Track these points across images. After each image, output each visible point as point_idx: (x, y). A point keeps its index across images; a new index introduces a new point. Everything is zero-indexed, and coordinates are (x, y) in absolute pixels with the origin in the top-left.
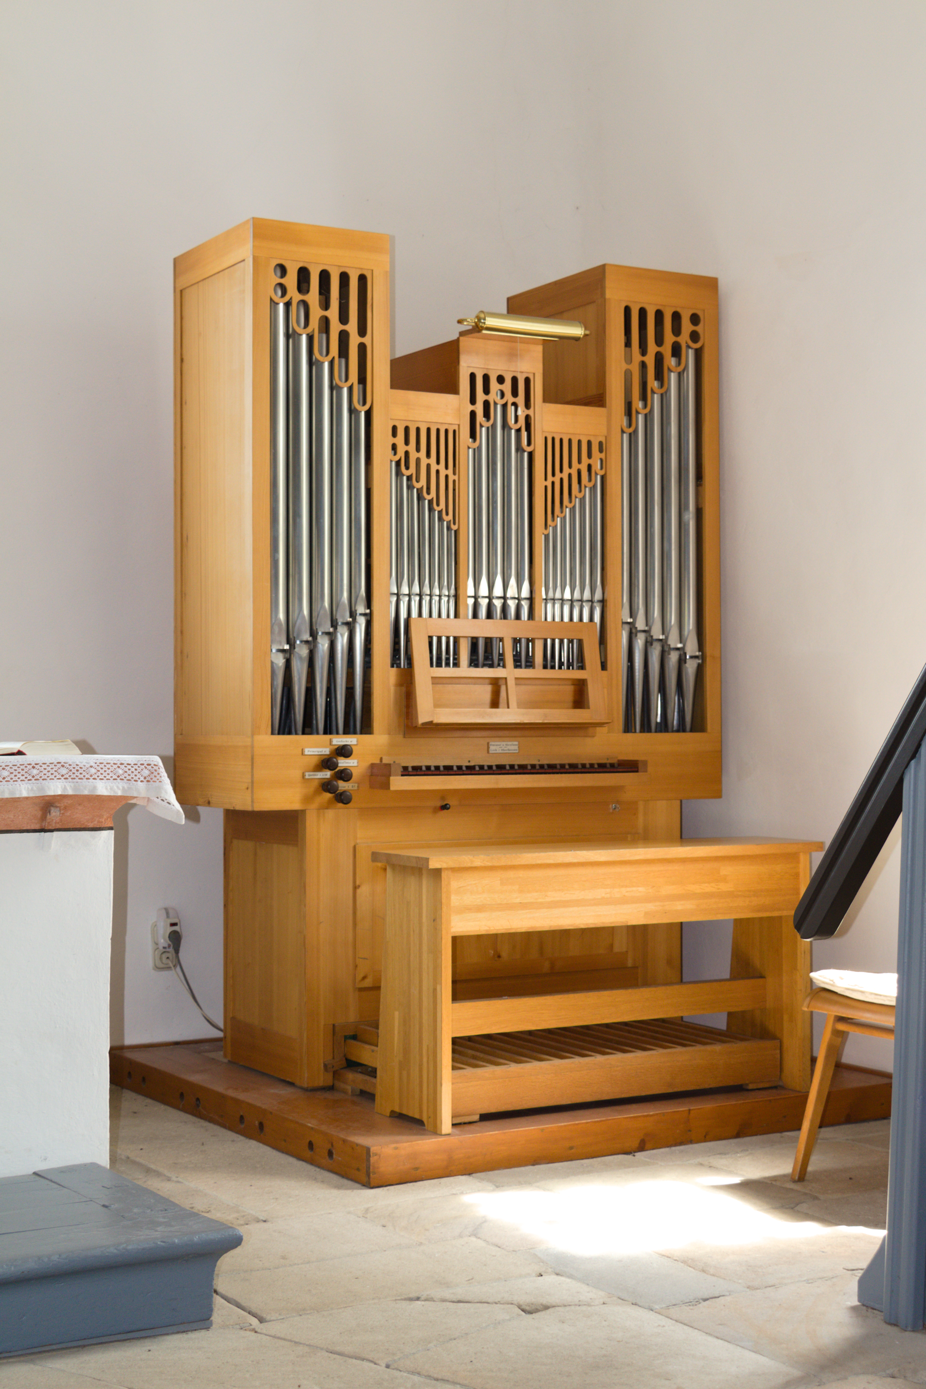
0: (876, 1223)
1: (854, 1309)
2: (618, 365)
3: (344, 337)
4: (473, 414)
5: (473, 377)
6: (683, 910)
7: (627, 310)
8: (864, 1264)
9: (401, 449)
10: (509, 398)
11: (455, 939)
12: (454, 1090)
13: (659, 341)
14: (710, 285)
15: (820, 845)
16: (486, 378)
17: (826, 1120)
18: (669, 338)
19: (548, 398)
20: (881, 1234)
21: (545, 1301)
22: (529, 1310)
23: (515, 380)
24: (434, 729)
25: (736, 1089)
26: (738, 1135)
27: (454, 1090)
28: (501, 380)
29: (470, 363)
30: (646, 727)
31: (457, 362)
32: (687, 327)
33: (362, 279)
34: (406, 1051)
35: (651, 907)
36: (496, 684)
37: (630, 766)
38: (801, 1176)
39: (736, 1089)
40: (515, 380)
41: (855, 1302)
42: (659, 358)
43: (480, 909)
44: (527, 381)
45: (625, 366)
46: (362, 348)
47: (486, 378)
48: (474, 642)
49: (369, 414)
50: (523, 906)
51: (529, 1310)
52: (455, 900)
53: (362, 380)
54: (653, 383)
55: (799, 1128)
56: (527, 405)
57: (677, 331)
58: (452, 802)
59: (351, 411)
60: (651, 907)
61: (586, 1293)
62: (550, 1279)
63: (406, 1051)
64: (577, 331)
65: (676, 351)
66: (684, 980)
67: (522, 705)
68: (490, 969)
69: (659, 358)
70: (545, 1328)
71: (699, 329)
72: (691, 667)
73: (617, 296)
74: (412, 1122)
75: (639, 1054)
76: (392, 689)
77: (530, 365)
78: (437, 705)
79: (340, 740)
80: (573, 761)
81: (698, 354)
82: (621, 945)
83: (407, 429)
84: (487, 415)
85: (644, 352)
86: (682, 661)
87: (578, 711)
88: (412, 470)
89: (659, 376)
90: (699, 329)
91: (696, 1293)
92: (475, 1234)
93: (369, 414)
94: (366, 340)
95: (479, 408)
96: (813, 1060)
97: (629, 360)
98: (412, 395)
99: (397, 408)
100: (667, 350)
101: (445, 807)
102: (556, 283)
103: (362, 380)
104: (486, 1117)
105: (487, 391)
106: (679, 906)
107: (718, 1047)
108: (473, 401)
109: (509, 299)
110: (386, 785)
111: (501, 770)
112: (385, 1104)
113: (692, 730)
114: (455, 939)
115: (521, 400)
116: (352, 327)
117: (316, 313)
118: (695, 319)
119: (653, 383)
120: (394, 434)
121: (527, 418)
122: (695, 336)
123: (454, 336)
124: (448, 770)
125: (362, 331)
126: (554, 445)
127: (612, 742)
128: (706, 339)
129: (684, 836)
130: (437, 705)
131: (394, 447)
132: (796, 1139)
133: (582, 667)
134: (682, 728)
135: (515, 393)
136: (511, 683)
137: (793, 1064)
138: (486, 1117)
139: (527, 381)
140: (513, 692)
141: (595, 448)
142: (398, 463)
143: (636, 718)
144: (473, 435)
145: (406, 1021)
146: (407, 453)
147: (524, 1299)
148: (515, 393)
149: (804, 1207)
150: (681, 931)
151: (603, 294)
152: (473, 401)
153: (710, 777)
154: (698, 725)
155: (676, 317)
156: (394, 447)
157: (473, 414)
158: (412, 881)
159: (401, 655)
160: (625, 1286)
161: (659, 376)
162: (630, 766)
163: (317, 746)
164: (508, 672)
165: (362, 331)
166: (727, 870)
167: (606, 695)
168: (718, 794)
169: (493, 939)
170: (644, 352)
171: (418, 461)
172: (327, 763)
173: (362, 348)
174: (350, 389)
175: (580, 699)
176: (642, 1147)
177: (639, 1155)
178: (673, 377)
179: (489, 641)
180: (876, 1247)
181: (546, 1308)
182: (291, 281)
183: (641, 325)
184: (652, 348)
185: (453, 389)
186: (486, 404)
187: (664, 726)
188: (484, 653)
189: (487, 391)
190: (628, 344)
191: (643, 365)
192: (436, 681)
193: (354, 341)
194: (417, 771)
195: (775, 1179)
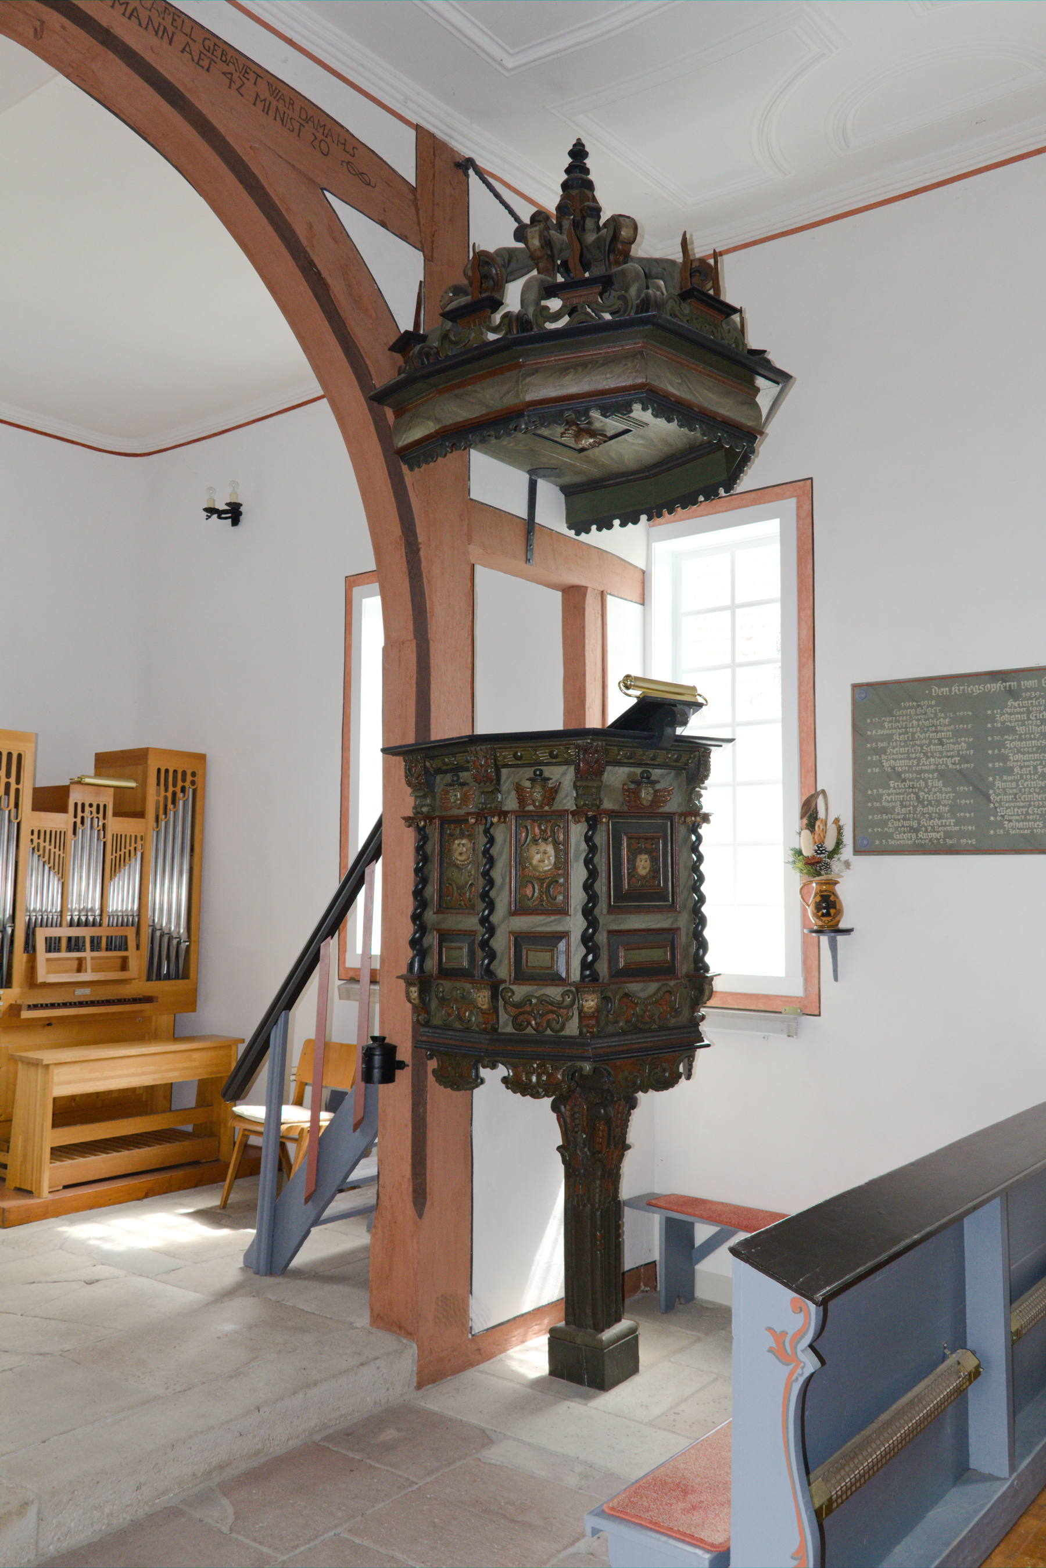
0: (252, 1227)
1: (241, 1268)
2: (153, 797)
4: (75, 823)
5: (76, 804)
6: (171, 1076)
7: (159, 770)
8: (247, 1248)
9: (36, 841)
10: (95, 814)
11: (54, 1099)
12: (51, 1175)
13: (175, 785)
14: (202, 758)
15: (243, 1041)
16: (83, 805)
17: (237, 1176)
18: (180, 784)
19: (116, 814)
20: (254, 1231)
21: (97, 1278)
22: (90, 1283)
23: (98, 806)
24: (45, 985)
25: (195, 1163)
26: (195, 1187)
27: (51, 1175)
28: (91, 805)
29: (76, 796)
30: (159, 977)
31: (68, 796)
32: (189, 778)
33: (20, 756)
34: (25, 1156)
35: (156, 1076)
36: (80, 960)
37: (149, 999)
38: (224, 1205)
39: (195, 1163)
40: (98, 806)
41: (242, 1265)
42: (174, 794)
43: (68, 1083)
44: (105, 806)
45: (156, 798)
46: (17, 791)
47: (83, 805)
48: (69, 939)
49: (19, 824)
50: (91, 1080)
51: (90, 1283)
52: (56, 1079)
53: (17, 806)
54: (170, 806)
55: (224, 1180)
56: (104, 818)
57: (184, 780)
58: (53, 1022)
59: (10, 821)
60: (156, 1076)
61: (116, 1272)
62: (99, 1267)
63: (25, 1156)
64: (133, 784)
65: (183, 789)
66: (173, 1108)
67: (94, 970)
68: (70, 1111)
69: (174, 794)
70: (97, 1290)
72: (184, 946)
73: (153, 765)
74: (24, 1192)
75: (147, 1149)
76: (24, 965)
77: (107, 799)
78: (48, 972)
80: (119, 997)
81: (194, 792)
82: (138, 1092)
84: (82, 823)
85: (166, 790)
86: (179, 943)
88: (41, 852)
89: (174, 802)
91: (169, 1263)
92: (61, 1248)
93: (19, 824)
95: (79, 820)
96: (234, 1143)
97: (158, 795)
98: (43, 814)
99: (32, 820)
100: (178, 789)
101: (49, 1025)
102: (122, 751)
103: (17, 806)
104: (65, 1187)
105: (83, 811)
106: (171, 1074)
107: (187, 1143)
108: (75, 816)
109: (96, 754)
110: (19, 1015)
111: (81, 1004)
112: (11, 1184)
113: (183, 978)
114: (54, 1099)
115: (101, 815)
118: (194, 774)
119: (170, 806)
120: (32, 834)
121: (104, 825)
122: (193, 783)
123: (67, 783)
124: (53, 1006)
125: (18, 782)
126: (118, 839)
127: (140, 987)
128: (199, 784)
129: (175, 1038)
130: (48, 972)
131: (32, 840)
132: (223, 1187)
133: (126, 949)
134: (177, 977)
135: (98, 812)
136: (89, 960)
137: (224, 1148)
138: (65, 1187)
139: (105, 806)
140: (89, 964)
141: (139, 839)
142: (33, 849)
143: (153, 973)
144: (75, 833)
145: (26, 1141)
146: (38, 844)
147: (87, 1278)
148: (98, 812)
149: (224, 1222)
150: (169, 1087)
151: (146, 762)
152: (75, 816)
153: (190, 1002)
154: (186, 976)
155: (184, 773)
156: (32, 840)
157: (75, 823)
158: (33, 1070)
159: (30, 946)
160: (136, 1264)
161: (174, 802)
162: (149, 999)
164: (87, 954)
165: (18, 782)
166: (195, 1055)
167: (137, 961)
168: (194, 1011)
169: (72, 1098)
170: (166, 790)
173: (17, 791)
174: (10, 811)
175: (124, 965)
176: (146, 1196)
177: (145, 1201)
178: (181, 802)
179: (77, 938)
180: (252, 1239)
181: (97, 1281)
184: (171, 789)
185: (64, 810)
186: (83, 818)
187: (168, 977)
188: (74, 944)
189: (83, 811)
190: (158, 784)
191: (166, 798)
192: (48, 960)
194: (35, 1007)
195: (211, 1208)
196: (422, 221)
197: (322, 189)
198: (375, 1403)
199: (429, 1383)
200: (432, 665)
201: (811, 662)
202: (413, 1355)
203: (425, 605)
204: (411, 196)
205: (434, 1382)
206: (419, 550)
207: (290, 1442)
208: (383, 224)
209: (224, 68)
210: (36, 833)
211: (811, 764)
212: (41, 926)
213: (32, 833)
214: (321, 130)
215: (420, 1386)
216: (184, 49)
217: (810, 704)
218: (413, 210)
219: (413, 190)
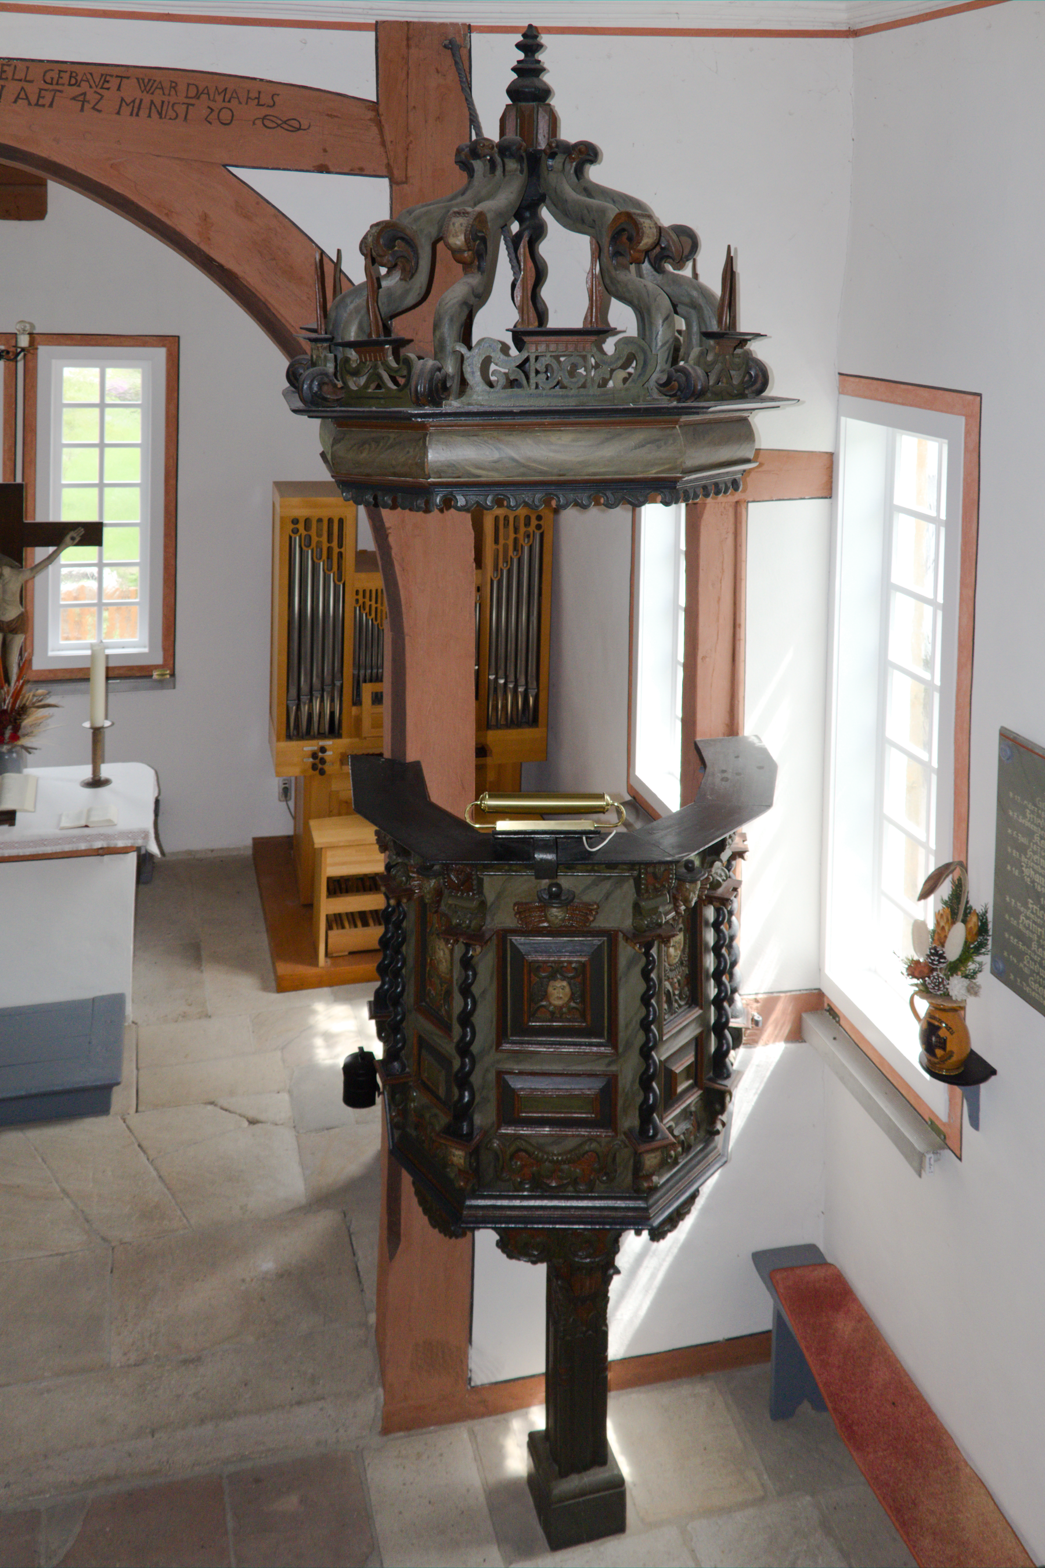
3: (330, 550)
32: (534, 522)
33: (341, 521)
46: (340, 555)
71: (541, 522)
79: (322, 743)
83: (364, 591)
87: (385, 679)
90: (541, 522)
94: (342, 550)
116: (335, 544)
117: (315, 539)
122: (539, 527)
125: (340, 545)
147: (252, 1114)
163: (310, 746)
165: (340, 545)
171: (370, 606)
172: (314, 755)
173: (340, 555)
182: (301, 527)
183: (390, 245)
184: (502, 541)
193: (336, 550)
196: (388, 137)
197: (224, 166)
198: (318, 1443)
199: (400, 1429)
200: (408, 664)
201: (970, 662)
202: (376, 1399)
203: (398, 595)
204: (371, 114)
205: (408, 1429)
206: (387, 536)
207: (196, 1468)
208: (323, 169)
209: (75, 91)
210: (361, 593)
211: (964, 810)
212: (365, 681)
213: (357, 592)
214: (219, 98)
215: (386, 1431)
216: (18, 97)
217: (966, 726)
218: (374, 130)
219: (374, 106)
